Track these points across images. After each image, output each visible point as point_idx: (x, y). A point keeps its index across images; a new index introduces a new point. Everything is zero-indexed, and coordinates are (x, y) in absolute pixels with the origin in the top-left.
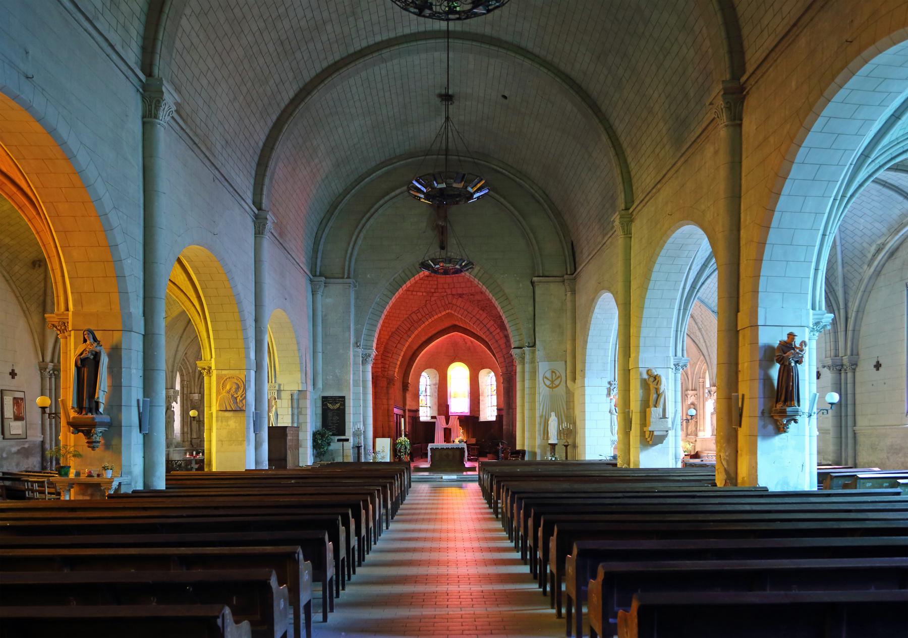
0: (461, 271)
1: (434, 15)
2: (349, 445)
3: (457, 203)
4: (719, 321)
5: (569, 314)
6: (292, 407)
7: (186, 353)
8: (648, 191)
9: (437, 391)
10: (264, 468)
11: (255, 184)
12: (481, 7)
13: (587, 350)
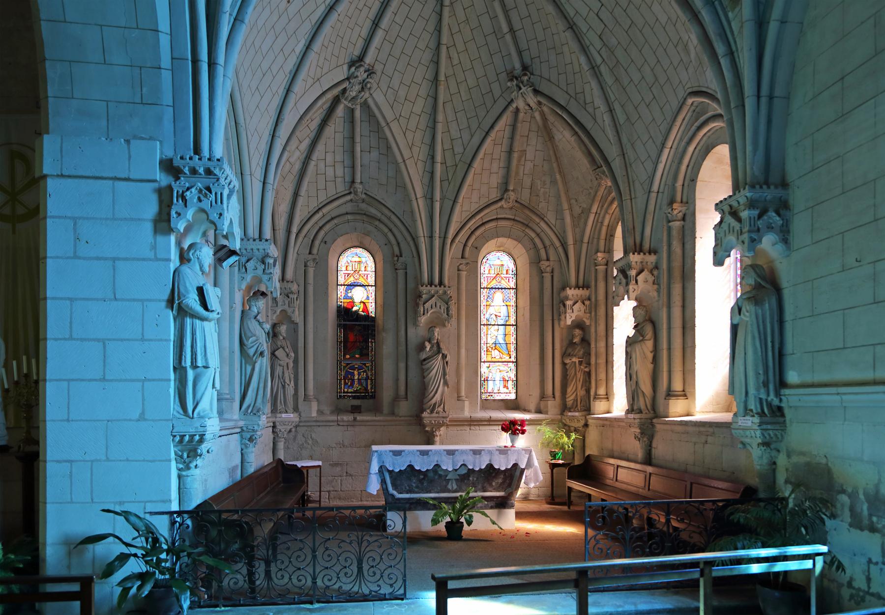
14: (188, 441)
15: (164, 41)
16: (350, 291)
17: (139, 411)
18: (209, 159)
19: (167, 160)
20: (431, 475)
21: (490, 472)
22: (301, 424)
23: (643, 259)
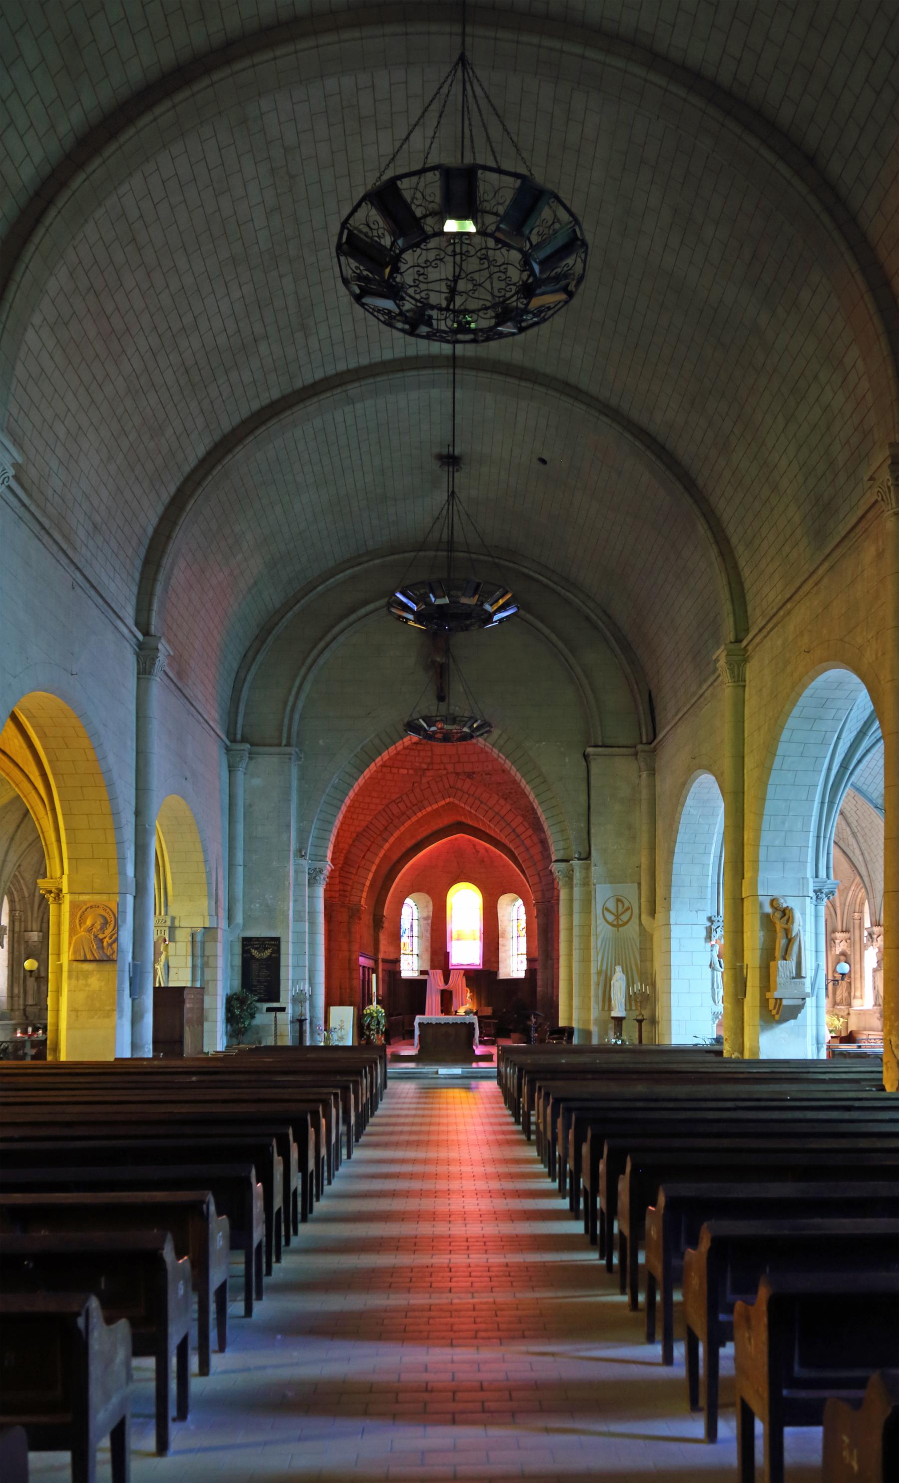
0: (472, 737)
1: (435, 335)
2: (285, 1018)
3: (466, 628)
4: (886, 823)
5: (644, 807)
6: (193, 955)
7: (19, 866)
8: (771, 614)
9: (429, 928)
10: (146, 1056)
11: (139, 593)
12: (509, 324)
13: (674, 866)
15: (710, 878)
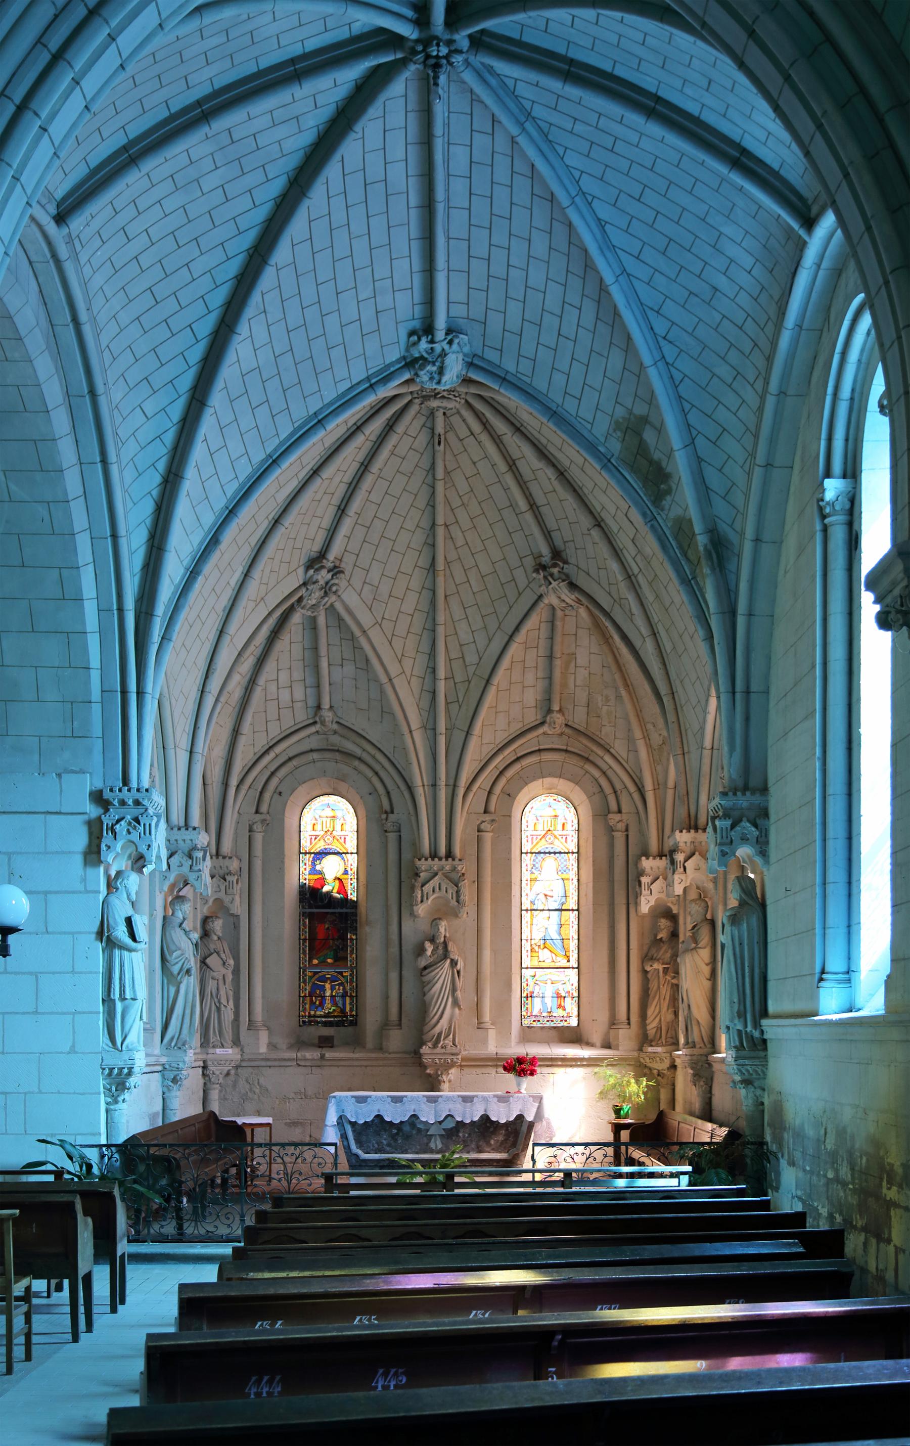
14: (117, 1074)
15: (95, 676)
16: (318, 862)
17: (70, 1044)
18: (138, 790)
19: (97, 791)
20: (406, 1128)
21: (486, 1126)
22: (244, 1064)
23: (695, 838)
